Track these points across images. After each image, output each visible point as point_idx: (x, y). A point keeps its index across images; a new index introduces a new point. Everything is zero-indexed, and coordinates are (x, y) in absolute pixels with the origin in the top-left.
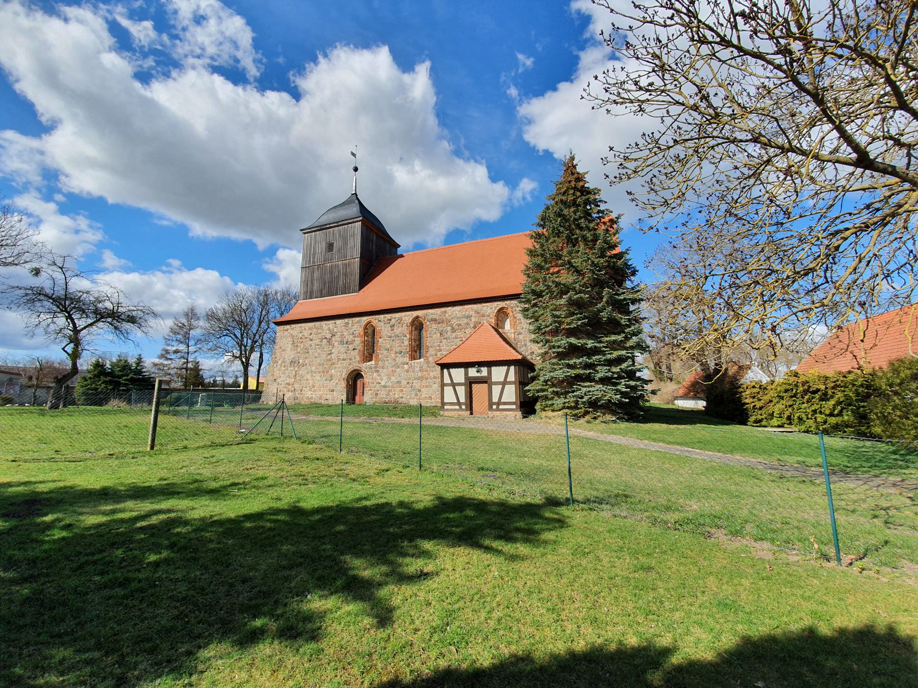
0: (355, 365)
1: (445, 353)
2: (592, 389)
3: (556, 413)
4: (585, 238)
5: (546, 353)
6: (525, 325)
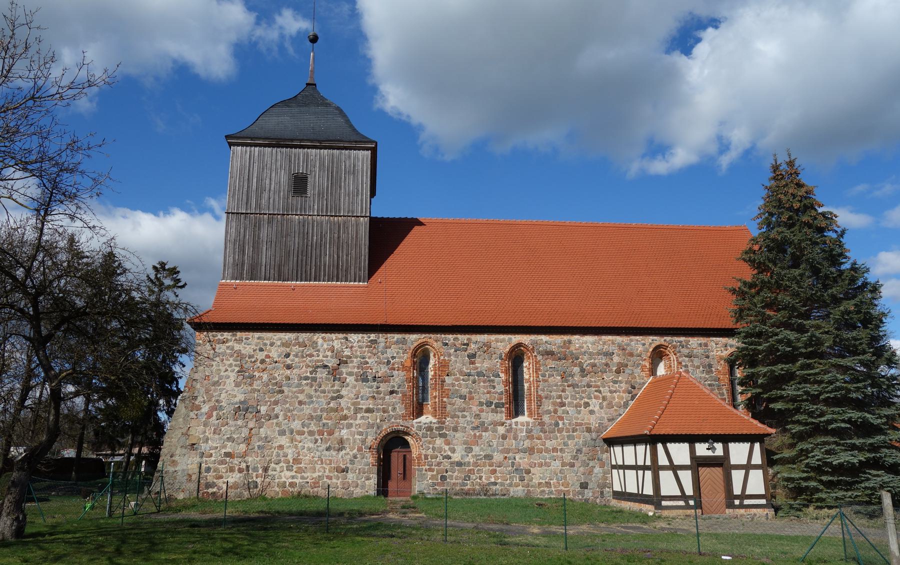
0: (399, 424)
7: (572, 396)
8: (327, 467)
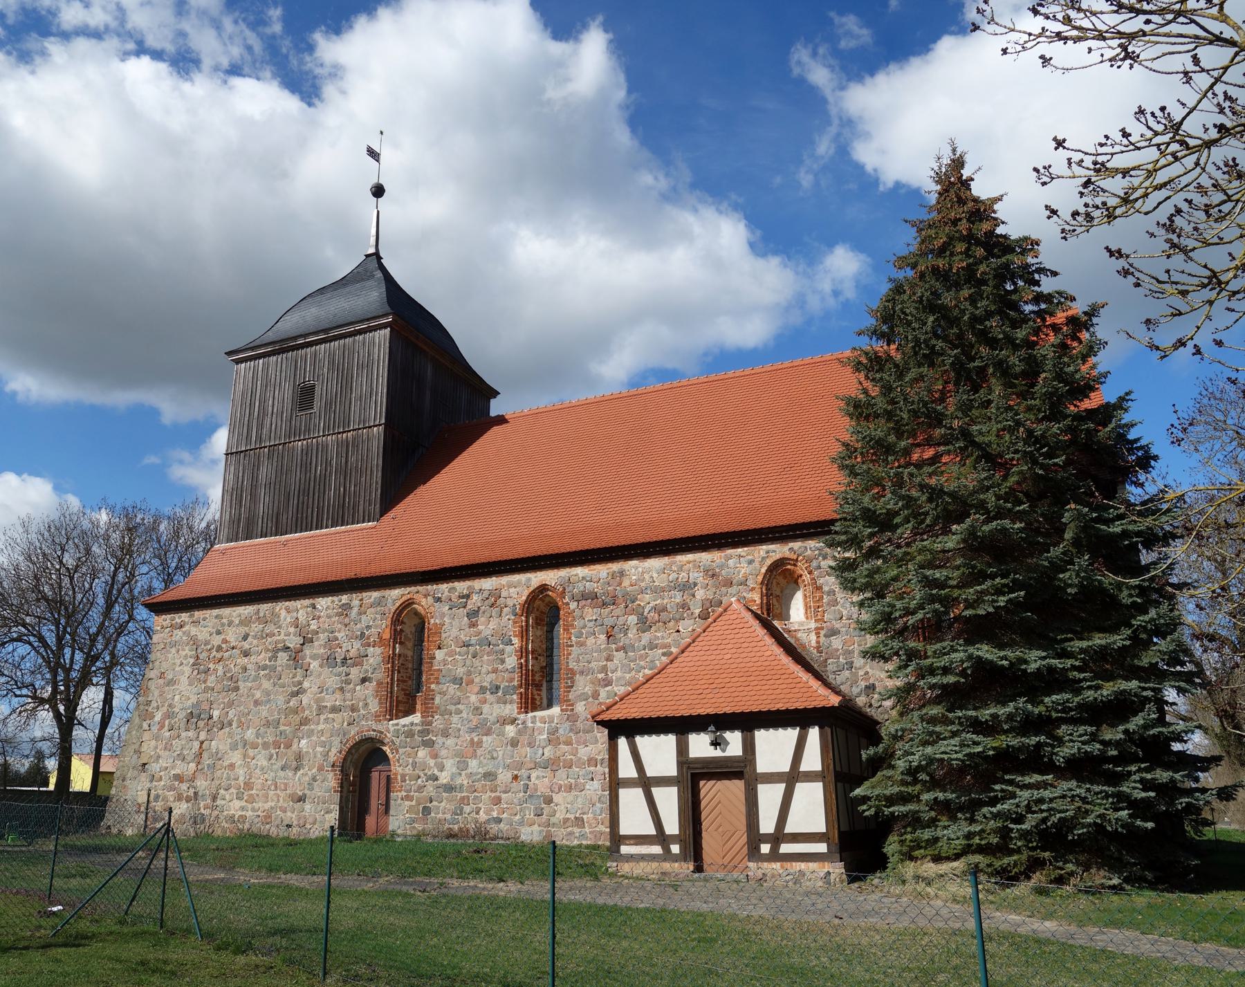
0: (369, 726)
1: (621, 690)
2: (1047, 794)
3: (945, 867)
4: (1003, 369)
5: (909, 688)
6: (846, 607)
7: (623, 666)
8: (282, 794)
